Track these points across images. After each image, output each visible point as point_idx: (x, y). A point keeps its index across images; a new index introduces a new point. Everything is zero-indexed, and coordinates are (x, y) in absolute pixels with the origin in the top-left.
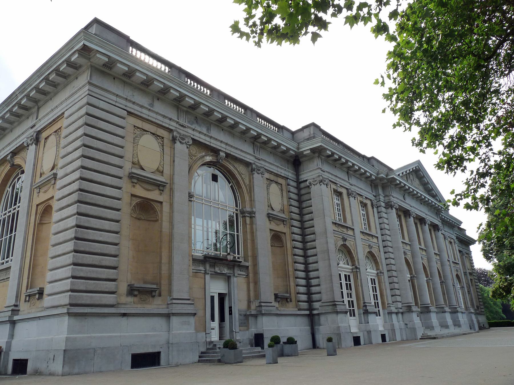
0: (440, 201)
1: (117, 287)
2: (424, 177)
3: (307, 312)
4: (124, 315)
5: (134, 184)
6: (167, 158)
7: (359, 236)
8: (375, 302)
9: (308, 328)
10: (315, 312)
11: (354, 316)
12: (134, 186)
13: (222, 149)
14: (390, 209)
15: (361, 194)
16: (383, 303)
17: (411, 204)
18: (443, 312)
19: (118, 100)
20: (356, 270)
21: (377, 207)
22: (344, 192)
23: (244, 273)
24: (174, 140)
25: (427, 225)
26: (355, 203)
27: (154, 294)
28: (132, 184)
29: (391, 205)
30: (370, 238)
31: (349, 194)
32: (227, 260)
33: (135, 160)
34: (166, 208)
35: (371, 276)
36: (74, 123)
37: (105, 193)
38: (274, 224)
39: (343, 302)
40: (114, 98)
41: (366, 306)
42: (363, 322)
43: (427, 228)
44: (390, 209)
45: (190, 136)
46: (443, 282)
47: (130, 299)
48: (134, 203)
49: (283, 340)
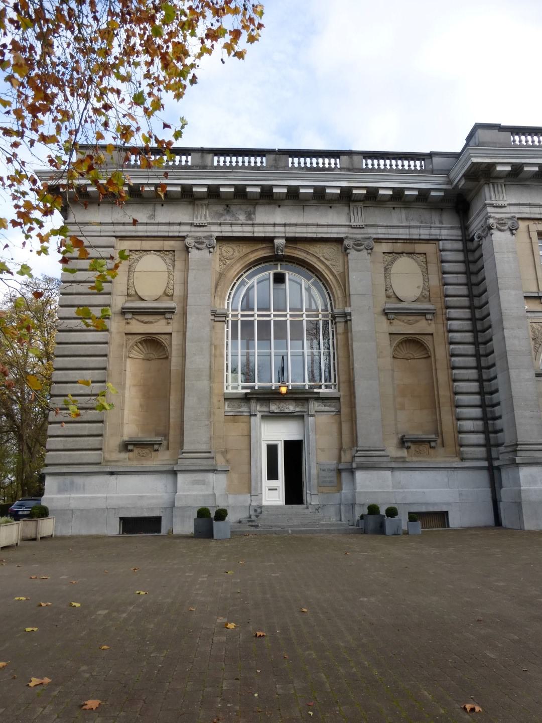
1: (101, 442)
3: (485, 464)
4: (112, 473)
5: (430, 322)
6: (178, 275)
9: (488, 491)
10: (496, 463)
12: (128, 323)
13: (277, 235)
19: (104, 228)
23: (333, 409)
24: (187, 249)
27: (433, 444)
28: (389, 321)
32: (280, 393)
33: (390, 293)
34: (176, 340)
37: (86, 341)
38: (401, 323)
40: (98, 228)
45: (370, 238)
47: (124, 455)
48: (131, 343)
49: (383, 512)
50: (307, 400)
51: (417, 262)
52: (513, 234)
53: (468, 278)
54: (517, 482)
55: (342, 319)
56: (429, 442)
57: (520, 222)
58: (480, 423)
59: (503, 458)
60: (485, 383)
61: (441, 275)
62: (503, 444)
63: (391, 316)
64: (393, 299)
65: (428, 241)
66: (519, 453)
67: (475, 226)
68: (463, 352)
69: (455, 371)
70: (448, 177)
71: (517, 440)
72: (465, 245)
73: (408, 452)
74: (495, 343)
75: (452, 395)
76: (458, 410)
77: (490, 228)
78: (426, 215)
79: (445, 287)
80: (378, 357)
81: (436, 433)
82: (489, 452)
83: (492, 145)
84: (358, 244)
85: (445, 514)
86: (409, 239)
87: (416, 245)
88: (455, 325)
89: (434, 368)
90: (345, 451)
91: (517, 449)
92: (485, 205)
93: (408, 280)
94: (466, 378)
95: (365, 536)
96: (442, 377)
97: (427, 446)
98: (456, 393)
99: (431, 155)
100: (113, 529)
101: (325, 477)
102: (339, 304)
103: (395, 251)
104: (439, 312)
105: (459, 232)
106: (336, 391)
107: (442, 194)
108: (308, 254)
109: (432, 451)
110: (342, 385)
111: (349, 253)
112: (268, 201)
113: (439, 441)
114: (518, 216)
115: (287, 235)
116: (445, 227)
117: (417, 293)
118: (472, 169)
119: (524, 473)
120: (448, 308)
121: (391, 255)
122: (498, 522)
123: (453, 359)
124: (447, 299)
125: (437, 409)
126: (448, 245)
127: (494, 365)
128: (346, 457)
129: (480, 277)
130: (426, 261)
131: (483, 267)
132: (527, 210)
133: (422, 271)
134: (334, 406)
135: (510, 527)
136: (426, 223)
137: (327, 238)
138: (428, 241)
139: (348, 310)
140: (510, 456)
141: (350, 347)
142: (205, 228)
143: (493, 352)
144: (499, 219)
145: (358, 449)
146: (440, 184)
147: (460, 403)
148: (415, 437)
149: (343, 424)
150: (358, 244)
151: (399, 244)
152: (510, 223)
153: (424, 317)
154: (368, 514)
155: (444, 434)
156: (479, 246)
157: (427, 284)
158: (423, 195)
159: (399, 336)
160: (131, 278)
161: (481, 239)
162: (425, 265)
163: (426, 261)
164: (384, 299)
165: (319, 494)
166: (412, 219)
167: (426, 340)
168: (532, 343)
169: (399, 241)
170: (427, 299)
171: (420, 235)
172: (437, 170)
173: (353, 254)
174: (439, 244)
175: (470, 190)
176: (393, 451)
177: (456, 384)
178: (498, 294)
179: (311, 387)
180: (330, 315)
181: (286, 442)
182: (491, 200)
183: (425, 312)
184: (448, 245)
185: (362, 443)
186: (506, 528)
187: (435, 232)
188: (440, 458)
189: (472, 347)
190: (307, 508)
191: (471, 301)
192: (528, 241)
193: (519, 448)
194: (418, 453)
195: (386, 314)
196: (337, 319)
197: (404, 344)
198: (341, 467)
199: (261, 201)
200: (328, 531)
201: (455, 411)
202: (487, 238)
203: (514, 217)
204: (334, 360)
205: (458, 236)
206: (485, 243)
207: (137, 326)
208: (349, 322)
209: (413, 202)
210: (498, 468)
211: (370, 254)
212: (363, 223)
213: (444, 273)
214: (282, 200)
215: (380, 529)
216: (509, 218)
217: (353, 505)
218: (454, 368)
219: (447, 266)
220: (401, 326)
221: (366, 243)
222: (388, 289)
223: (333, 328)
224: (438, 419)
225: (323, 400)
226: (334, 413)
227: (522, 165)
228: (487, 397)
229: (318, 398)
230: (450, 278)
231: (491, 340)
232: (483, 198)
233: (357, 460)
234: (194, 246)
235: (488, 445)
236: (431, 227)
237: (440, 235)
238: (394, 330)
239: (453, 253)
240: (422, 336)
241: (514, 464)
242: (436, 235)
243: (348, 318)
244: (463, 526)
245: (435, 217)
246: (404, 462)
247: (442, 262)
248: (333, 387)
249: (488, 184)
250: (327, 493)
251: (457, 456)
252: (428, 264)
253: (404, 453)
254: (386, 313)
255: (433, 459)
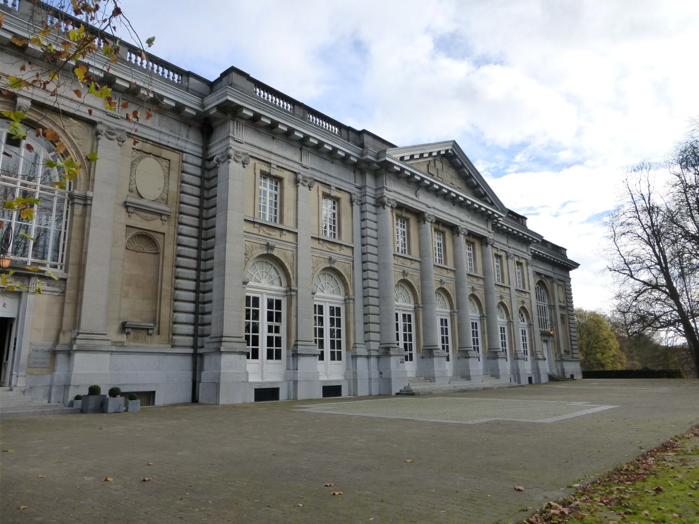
0: (492, 204)
2: (463, 166)
5: (164, 222)
7: (514, 294)
8: (524, 351)
10: (200, 351)
11: (340, 358)
14: (381, 208)
15: (327, 182)
16: (348, 342)
17: (424, 202)
18: (466, 358)
20: (510, 322)
21: (362, 204)
22: (287, 176)
23: (57, 289)
25: (462, 237)
26: (512, 263)
27: (150, 332)
28: (127, 214)
29: (383, 203)
30: (523, 294)
31: (507, 257)
33: (133, 187)
35: (330, 302)
36: (353, 235)
39: (398, 344)
41: (356, 347)
42: (291, 368)
43: (462, 239)
44: (381, 208)
45: (123, 131)
46: (484, 316)
49: (105, 391)
50: (29, 276)
51: (161, 165)
52: (244, 167)
53: (202, 192)
54: (218, 366)
55: (82, 202)
56: (148, 329)
57: (251, 159)
58: (192, 316)
59: (207, 345)
60: (201, 283)
61: (179, 183)
62: (209, 335)
63: (131, 210)
64: (135, 194)
65: (174, 150)
66: (223, 344)
67: (216, 150)
68: (187, 254)
69: (178, 270)
70: (202, 101)
71: (222, 333)
72: (203, 163)
73: (127, 337)
74: (216, 252)
75: (173, 290)
76: (177, 303)
77: (229, 157)
78: (176, 126)
79: (182, 195)
80: (113, 246)
81: (154, 321)
82: (195, 342)
83: (241, 89)
84: (110, 133)
85: (153, 394)
86: (158, 143)
87: (163, 150)
88: (185, 229)
89: (161, 264)
90: (64, 333)
91: (223, 340)
92: (229, 137)
93: (152, 180)
94: (186, 276)
95: (83, 417)
96: (167, 273)
97: (145, 332)
98: (176, 289)
99: (189, 74)
100: (319, 394)
101: (37, 358)
102: (80, 186)
103: (144, 150)
104: (173, 215)
105: (200, 151)
106: (63, 271)
107: (194, 113)
108: (54, 125)
109: (148, 338)
110: (70, 267)
111: (100, 139)
112: (17, 53)
113: (156, 329)
114: (250, 154)
115: (34, 98)
116: (191, 143)
117: (157, 194)
118: (225, 104)
119: (225, 358)
120: (181, 213)
121: (139, 152)
122: (195, 399)
123: (179, 259)
124: (182, 205)
125: (158, 301)
126: (191, 159)
127: (212, 269)
128: (65, 339)
129: (211, 193)
130: (169, 167)
131: (216, 186)
132: (256, 150)
133: (165, 176)
134: (59, 287)
135: (206, 402)
136: (175, 133)
137: (80, 116)
138: (174, 150)
139: (89, 194)
140: (216, 345)
141: (86, 231)
142: (117, 120)
143: (212, 258)
144: (237, 152)
145: (80, 332)
146: (194, 104)
147: (179, 298)
148: (137, 324)
149: (66, 306)
150: (110, 133)
151: (148, 145)
152: (243, 157)
153: (160, 217)
154: (89, 394)
155: (161, 324)
156: (215, 167)
157: (167, 188)
158: (178, 109)
159: (134, 230)
160: (133, 175)
161: (219, 163)
162: (167, 170)
163: (169, 167)
164: (126, 192)
165: (28, 376)
166: (164, 126)
167: (158, 238)
168: (244, 256)
169: (149, 142)
170: (165, 202)
171: (168, 142)
172: (192, 90)
173: (103, 141)
174: (182, 155)
175: (216, 119)
176: (114, 335)
177: (178, 281)
178: (226, 213)
179: (33, 263)
180: (67, 195)
181: (281, 337)
182: (233, 134)
183: (162, 212)
184: (191, 159)
185: (84, 325)
186: (201, 404)
187: (181, 144)
188: (156, 343)
189: (195, 251)
190: (11, 390)
191: (201, 212)
192: (253, 175)
193: (224, 339)
194: (136, 339)
195: (127, 207)
196: (76, 201)
197: (137, 238)
198: (58, 348)
199: (7, 49)
200: (43, 413)
201: (174, 304)
202: (224, 164)
203: (247, 154)
204: (64, 240)
205: (199, 153)
206: (222, 167)
207: (137, 221)
208: (88, 207)
209: (168, 110)
210: (202, 355)
211: (120, 145)
212: (119, 114)
213: (183, 182)
214: (35, 58)
215: (102, 408)
216: (244, 154)
217: (67, 386)
218: (178, 267)
219: (187, 177)
220: (137, 221)
221: (119, 134)
222: (132, 183)
223: (68, 208)
224: (158, 309)
225: (47, 279)
226: (57, 294)
227: (324, 143)
228: (201, 295)
229: (43, 277)
230: (187, 188)
231: (213, 248)
232: (227, 130)
233: (78, 342)
234: (105, 134)
235: (195, 335)
236: (179, 138)
237: (185, 148)
238: (131, 222)
239: (193, 166)
240: (155, 234)
241: (219, 352)
242: (181, 147)
243: (89, 202)
244: (166, 403)
245: (184, 131)
246: (123, 346)
247: (183, 172)
248: (59, 267)
249: (234, 120)
250: (37, 375)
251: (169, 343)
252: (171, 171)
253: (123, 338)
254: (126, 205)
255: (149, 345)
